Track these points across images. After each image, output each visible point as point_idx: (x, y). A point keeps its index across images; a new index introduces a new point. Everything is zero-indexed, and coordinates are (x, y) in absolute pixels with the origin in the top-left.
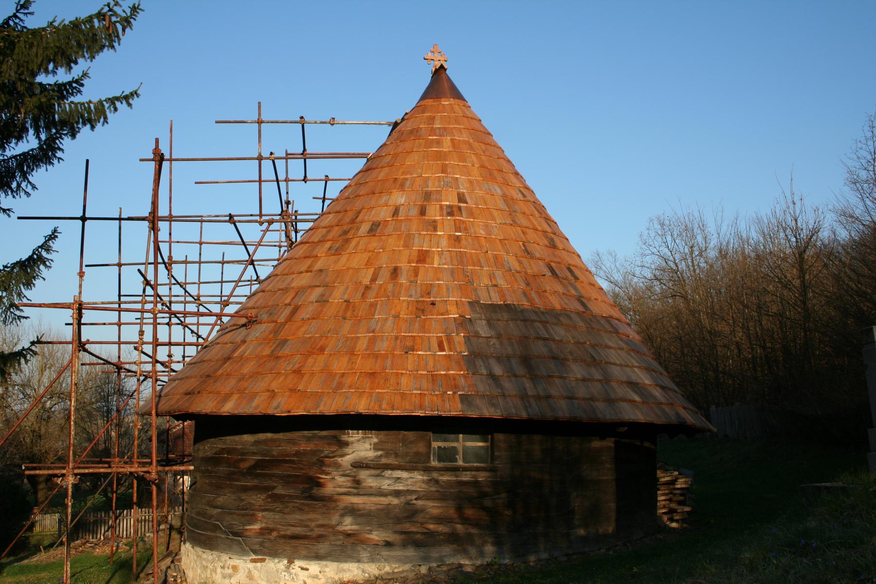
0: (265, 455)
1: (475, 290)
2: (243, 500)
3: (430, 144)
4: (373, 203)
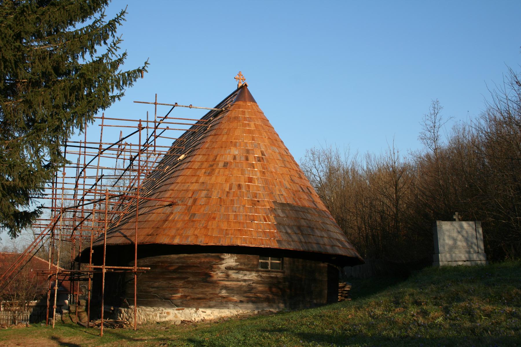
1: (274, 196)
2: (171, 284)
3: (245, 125)
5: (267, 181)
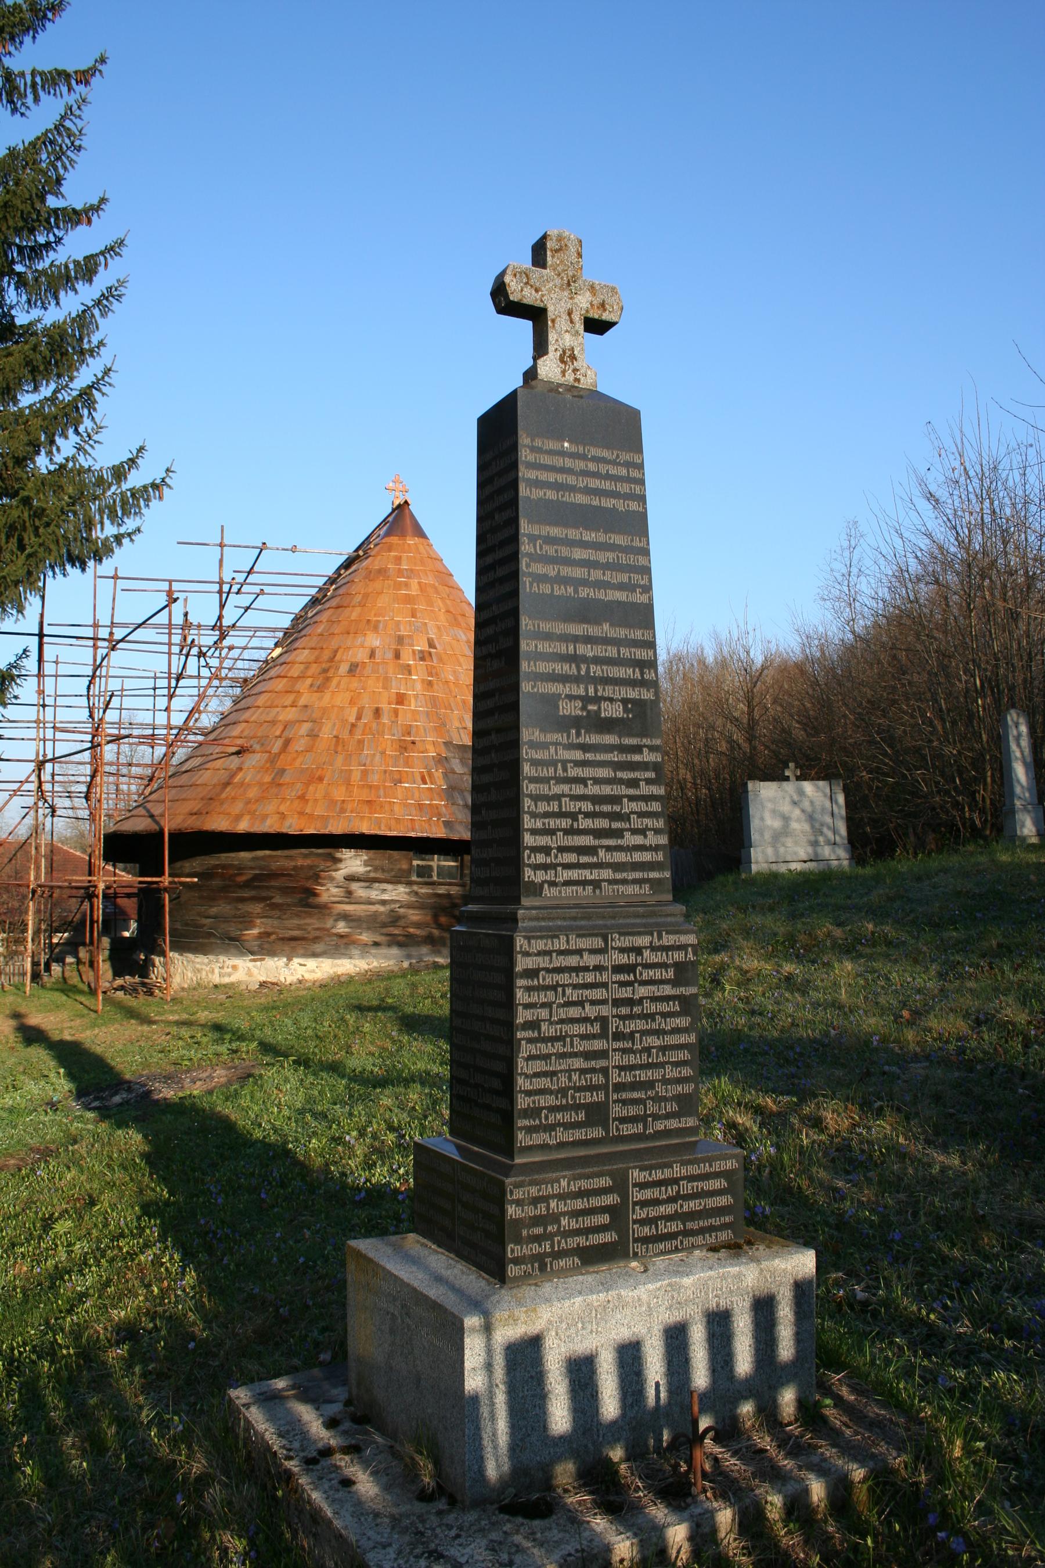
0: (261, 868)
1: (448, 731)
3: (398, 586)
4: (349, 643)
5: (435, 701)
